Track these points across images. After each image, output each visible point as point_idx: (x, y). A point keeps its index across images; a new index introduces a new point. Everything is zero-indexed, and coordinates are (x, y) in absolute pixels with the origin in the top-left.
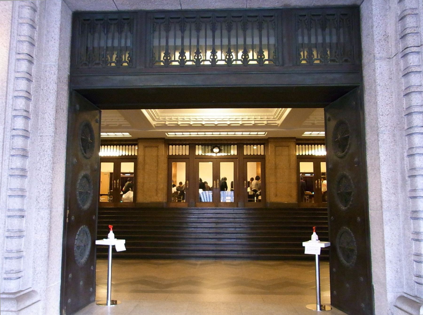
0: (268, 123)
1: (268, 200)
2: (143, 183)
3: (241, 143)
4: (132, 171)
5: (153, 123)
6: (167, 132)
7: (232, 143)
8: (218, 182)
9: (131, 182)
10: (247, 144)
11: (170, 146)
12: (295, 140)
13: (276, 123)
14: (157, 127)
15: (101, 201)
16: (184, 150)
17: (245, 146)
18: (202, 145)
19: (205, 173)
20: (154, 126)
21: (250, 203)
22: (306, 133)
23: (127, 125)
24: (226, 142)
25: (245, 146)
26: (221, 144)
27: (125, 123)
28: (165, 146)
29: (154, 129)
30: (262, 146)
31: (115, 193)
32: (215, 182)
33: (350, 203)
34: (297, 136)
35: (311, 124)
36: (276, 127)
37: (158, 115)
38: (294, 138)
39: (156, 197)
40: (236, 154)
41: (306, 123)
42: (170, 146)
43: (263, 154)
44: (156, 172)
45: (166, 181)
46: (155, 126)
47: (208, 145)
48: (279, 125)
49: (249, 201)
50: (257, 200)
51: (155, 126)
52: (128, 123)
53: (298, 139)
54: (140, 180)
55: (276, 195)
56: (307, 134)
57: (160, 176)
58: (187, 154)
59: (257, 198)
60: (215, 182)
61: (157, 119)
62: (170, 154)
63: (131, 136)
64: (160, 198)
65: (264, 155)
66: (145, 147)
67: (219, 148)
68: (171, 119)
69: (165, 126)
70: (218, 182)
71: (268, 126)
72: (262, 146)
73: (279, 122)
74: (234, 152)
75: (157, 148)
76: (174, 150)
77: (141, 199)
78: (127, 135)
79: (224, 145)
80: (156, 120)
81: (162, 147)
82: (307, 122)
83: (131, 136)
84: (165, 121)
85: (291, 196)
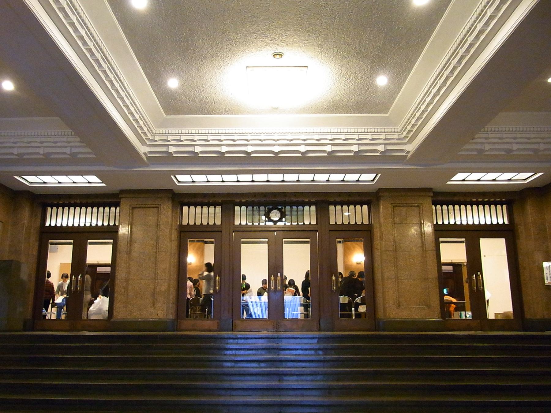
0: (386, 151)
1: (380, 314)
2: (127, 281)
3: (323, 199)
4: (109, 261)
5: (142, 150)
6: (176, 173)
7: (306, 200)
8: (279, 278)
9: (101, 281)
10: (335, 204)
11: (185, 208)
12: (432, 195)
13: (402, 151)
14: (153, 160)
15: (55, 318)
16: (211, 216)
17: (332, 208)
18: (247, 205)
19: (254, 263)
20: (144, 157)
21: (344, 322)
22: (460, 176)
23: (89, 156)
24: (294, 199)
25: (332, 208)
26: (285, 204)
27: (84, 151)
28: (173, 206)
29: (147, 165)
30: (365, 207)
31: (76, 301)
32: (272, 278)
33: (59, 299)
34: (437, 185)
35: (475, 153)
36: (401, 159)
37: (150, 130)
38: (430, 189)
39: (152, 310)
40: (314, 222)
41: (465, 150)
42: (185, 208)
43: (366, 222)
44: (153, 259)
45: (174, 276)
46: (148, 158)
47: (259, 205)
48: (409, 155)
49: (343, 316)
50: (356, 315)
51: (148, 158)
52: (90, 151)
53: (436, 194)
54: (121, 275)
55: (399, 306)
56: (459, 178)
57: (163, 266)
58: (218, 223)
59: (356, 310)
60: (272, 278)
61: (148, 139)
62: (185, 223)
63: (104, 185)
64: (161, 311)
65: (370, 224)
66: (133, 208)
67: (280, 210)
68: (181, 141)
69: (168, 158)
70: (279, 278)
71: (385, 157)
72: (365, 207)
73: (411, 148)
74: (309, 216)
75: (155, 210)
76: (192, 215)
77: (120, 314)
78: (93, 181)
79: (291, 204)
80: (148, 143)
81: (167, 210)
82: (470, 148)
83: (104, 185)
84: (168, 145)
85: (429, 306)
